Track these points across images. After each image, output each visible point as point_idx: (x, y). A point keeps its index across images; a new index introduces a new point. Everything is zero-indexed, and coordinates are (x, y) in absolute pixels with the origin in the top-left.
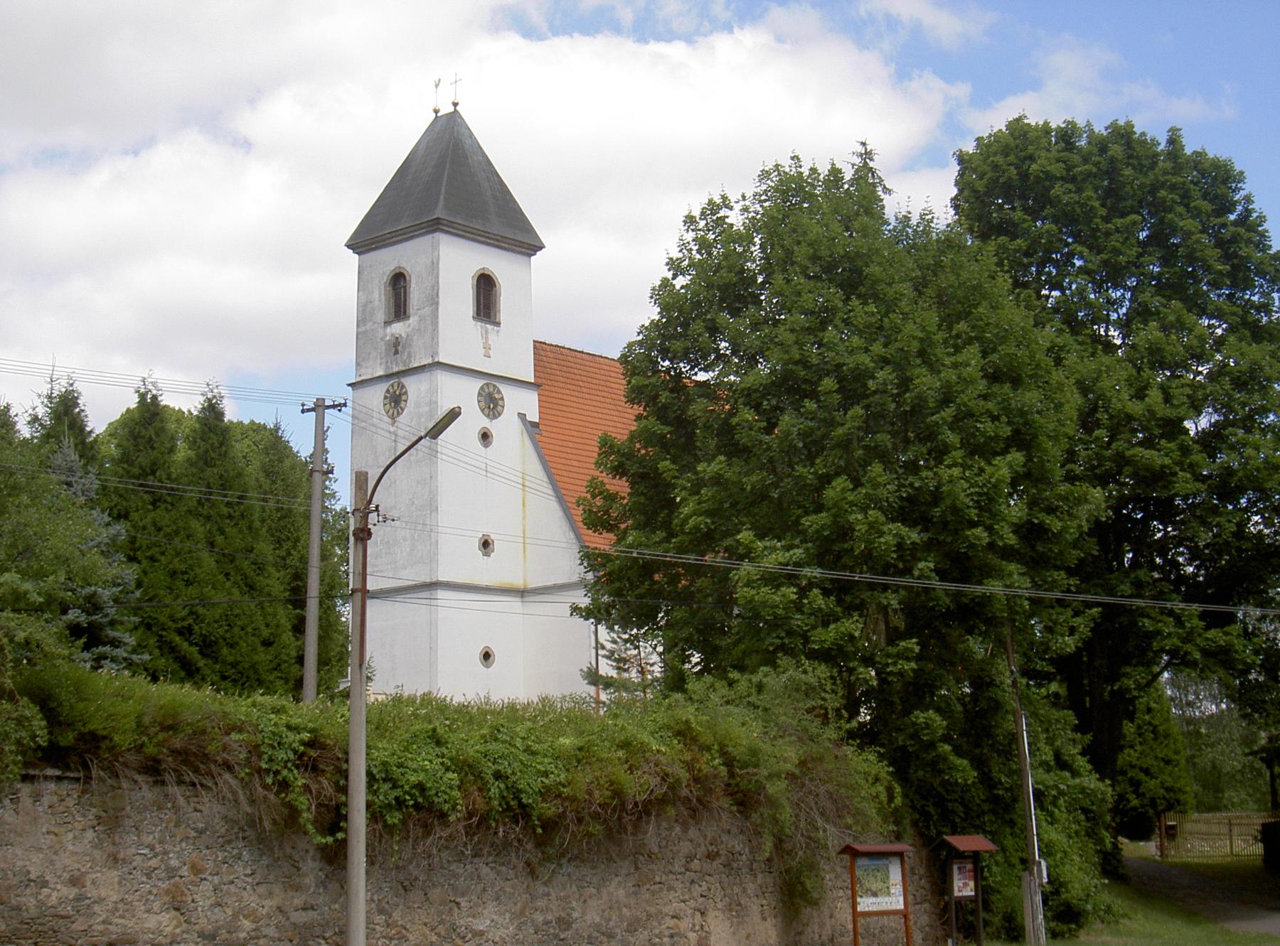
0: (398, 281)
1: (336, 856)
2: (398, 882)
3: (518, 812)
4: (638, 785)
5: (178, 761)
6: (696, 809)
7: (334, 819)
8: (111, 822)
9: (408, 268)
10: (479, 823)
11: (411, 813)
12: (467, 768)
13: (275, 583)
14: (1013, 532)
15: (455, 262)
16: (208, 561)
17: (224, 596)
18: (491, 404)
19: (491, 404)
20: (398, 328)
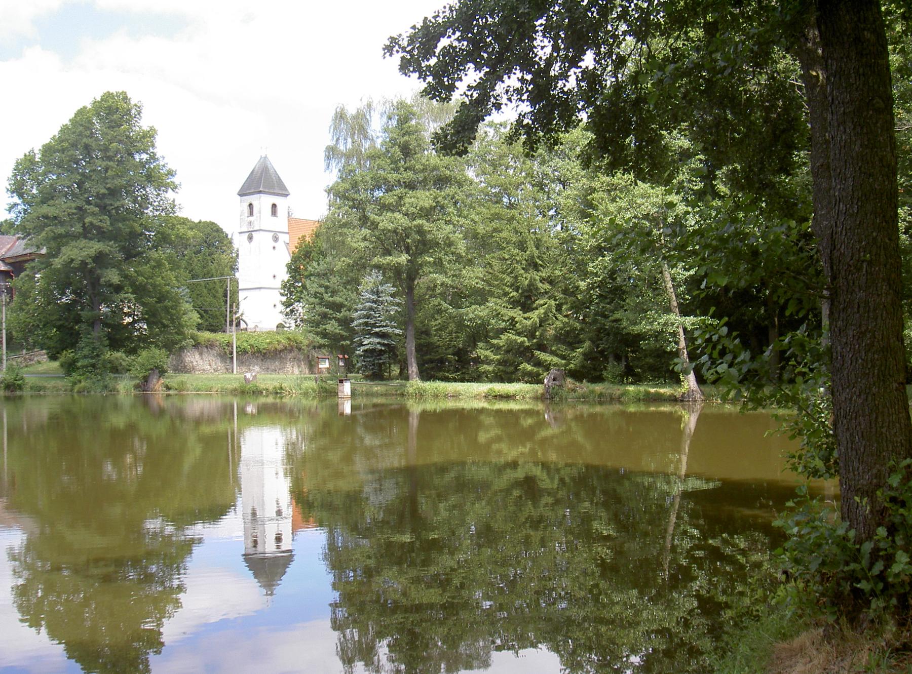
0: (251, 205)
1: (28, 428)
2: (241, 363)
3: (259, 351)
4: (280, 347)
5: (210, 345)
6: (291, 351)
7: (232, 353)
8: (201, 354)
9: (253, 203)
10: (253, 354)
11: (242, 352)
12: (252, 346)
13: (221, 291)
14: (611, 169)
15: (263, 202)
16: (205, 291)
17: (210, 299)
18: (276, 239)
19: (276, 239)
20: (251, 219)
